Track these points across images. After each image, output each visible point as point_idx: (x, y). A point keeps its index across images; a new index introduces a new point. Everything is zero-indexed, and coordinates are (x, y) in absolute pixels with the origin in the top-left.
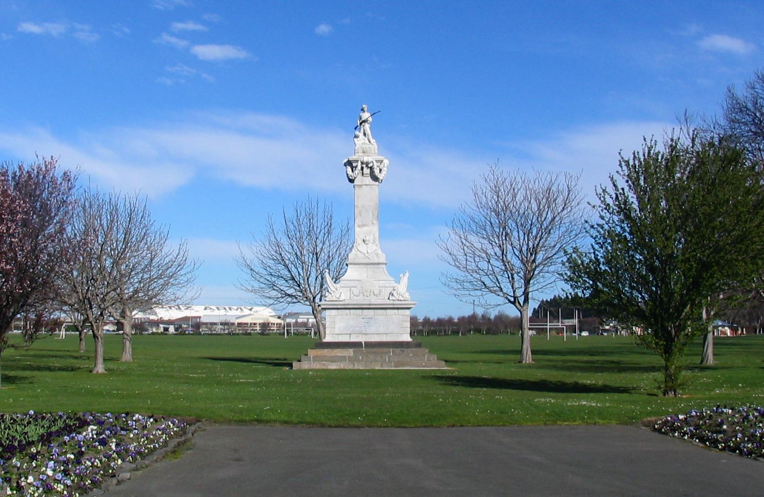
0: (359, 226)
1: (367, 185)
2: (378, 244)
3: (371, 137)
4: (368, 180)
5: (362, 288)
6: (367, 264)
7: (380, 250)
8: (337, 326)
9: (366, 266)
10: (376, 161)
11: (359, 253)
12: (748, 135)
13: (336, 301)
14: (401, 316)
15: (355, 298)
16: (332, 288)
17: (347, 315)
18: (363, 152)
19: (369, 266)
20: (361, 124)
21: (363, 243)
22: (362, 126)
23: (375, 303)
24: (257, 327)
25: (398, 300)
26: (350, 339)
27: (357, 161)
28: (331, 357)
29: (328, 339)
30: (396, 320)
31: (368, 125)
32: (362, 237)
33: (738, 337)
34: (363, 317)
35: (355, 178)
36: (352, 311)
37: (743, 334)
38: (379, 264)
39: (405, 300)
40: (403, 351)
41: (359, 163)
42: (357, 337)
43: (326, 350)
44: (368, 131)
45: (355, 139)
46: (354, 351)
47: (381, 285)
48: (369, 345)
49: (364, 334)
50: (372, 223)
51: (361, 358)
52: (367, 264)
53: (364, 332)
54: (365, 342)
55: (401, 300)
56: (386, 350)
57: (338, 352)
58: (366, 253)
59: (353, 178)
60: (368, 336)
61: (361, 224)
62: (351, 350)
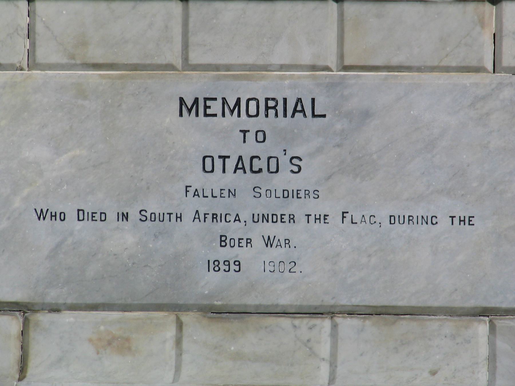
34: (192, 87)
49: (217, 312)
53: (209, 284)
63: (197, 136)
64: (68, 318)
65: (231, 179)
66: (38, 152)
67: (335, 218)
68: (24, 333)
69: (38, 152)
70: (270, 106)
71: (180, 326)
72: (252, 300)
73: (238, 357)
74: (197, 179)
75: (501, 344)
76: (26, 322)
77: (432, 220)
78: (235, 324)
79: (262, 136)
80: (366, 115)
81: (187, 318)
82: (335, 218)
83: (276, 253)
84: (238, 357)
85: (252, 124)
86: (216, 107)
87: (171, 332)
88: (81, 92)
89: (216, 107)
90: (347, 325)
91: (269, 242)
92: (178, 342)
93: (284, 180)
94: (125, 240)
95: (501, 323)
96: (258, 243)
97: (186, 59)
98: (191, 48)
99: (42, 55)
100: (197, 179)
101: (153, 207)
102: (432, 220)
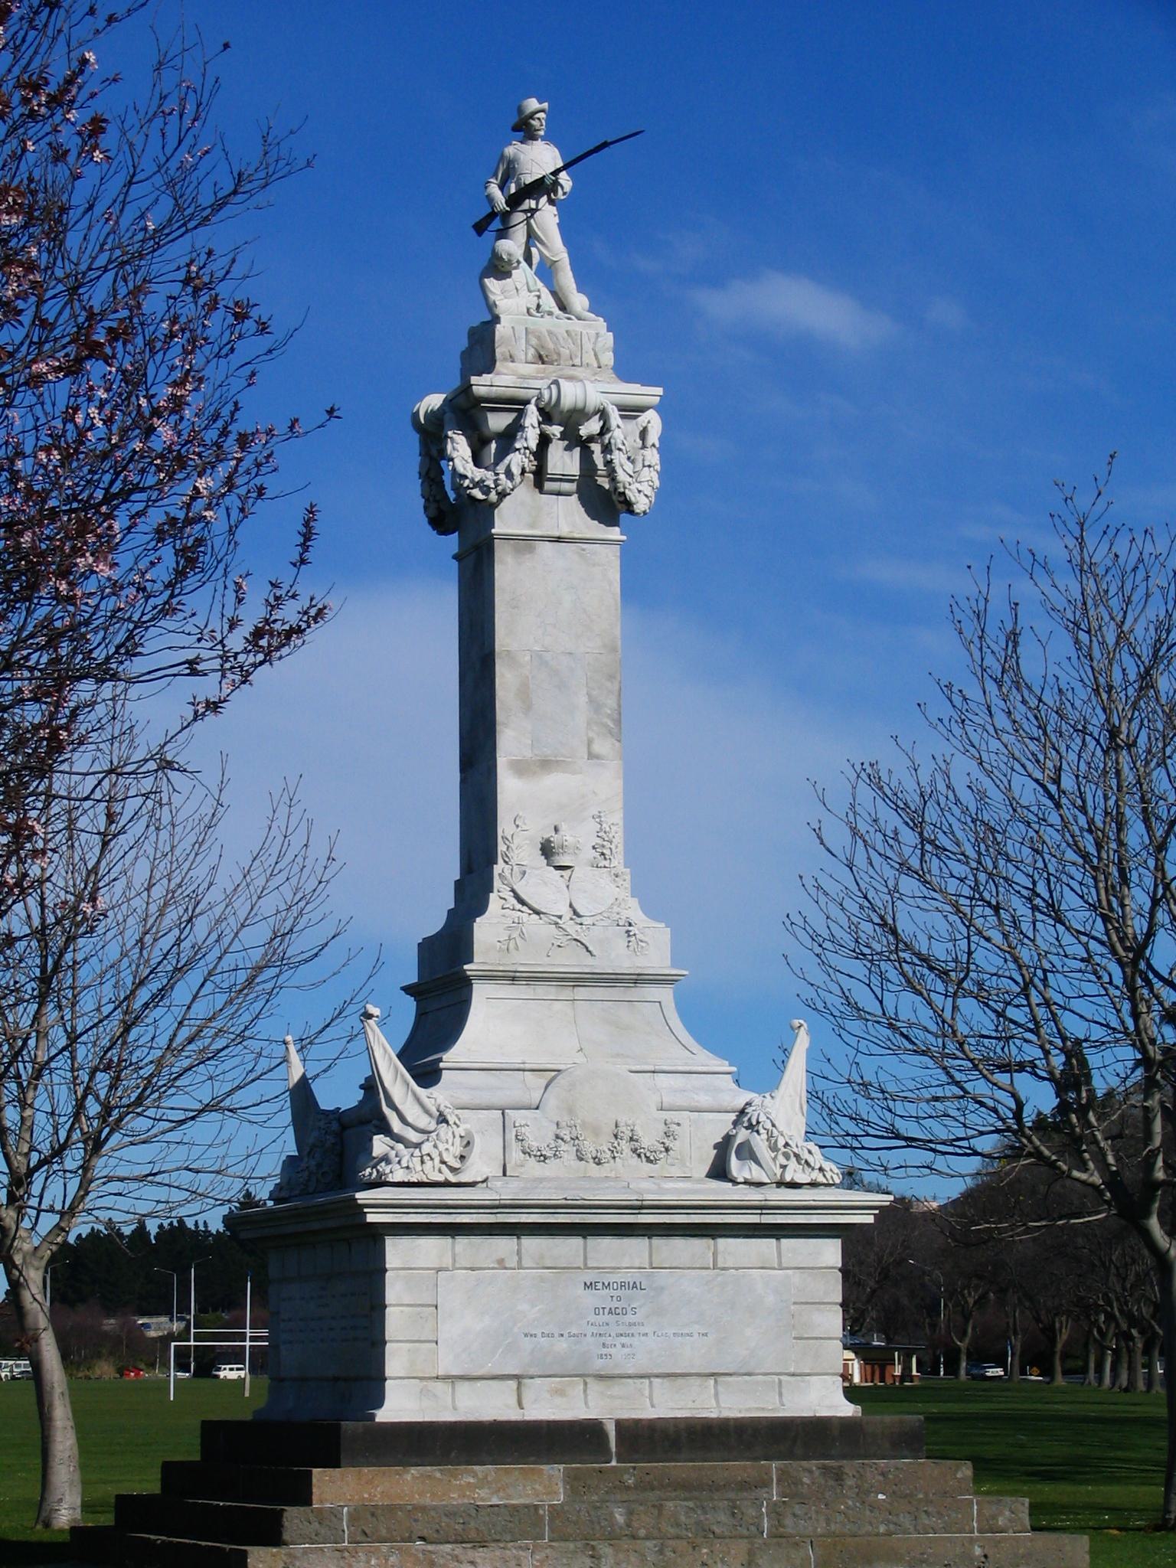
0: (521, 768)
1: (559, 540)
2: (621, 869)
3: (567, 279)
4: (567, 514)
5: (571, 1111)
6: (578, 980)
7: (634, 903)
8: (449, 1331)
9: (567, 993)
10: (621, 408)
11: (526, 917)
12: (107, 490)
13: (447, 1184)
14: (796, 1277)
15: (534, 1169)
16: (412, 1113)
17: (501, 1264)
18: (541, 359)
19: (582, 993)
20: (514, 201)
21: (543, 860)
22: (518, 217)
23: (669, 1198)
24: (242, 1337)
25: (780, 1184)
26: (520, 1405)
27: (516, 405)
28: (451, 1513)
29: (399, 1406)
30: (770, 1299)
31: (554, 209)
32: (536, 829)
33: (893, 1386)
34: (589, 1276)
35: (502, 495)
36: (530, 1243)
37: (911, 1378)
38: (638, 980)
39: (814, 1185)
40: (839, 1477)
41: (532, 417)
42: (560, 1392)
43: (413, 1470)
44: (556, 248)
45: (491, 283)
46: (571, 1479)
47: (667, 1100)
48: (646, 1439)
49: (600, 1377)
50: (591, 756)
51: (620, 1519)
52: (578, 980)
53: (598, 1365)
54: (619, 1424)
55: (794, 1185)
56: (739, 1468)
57: (483, 1482)
58: (567, 913)
59: (493, 497)
60: (617, 1389)
61: (528, 754)
62: (555, 1471)
63: (590, 1299)
64: (538, 1381)
65: (607, 1318)
66: (524, 1307)
67: (651, 1334)
68: (519, 1388)
69: (524, 1307)
70: (622, 1285)
71: (585, 1384)
72: (617, 1372)
73: (611, 1397)
74: (592, 1318)
75: (720, 1389)
76: (519, 1384)
77: (690, 1335)
78: (609, 1382)
79: (619, 1298)
80: (662, 1288)
81: (588, 1380)
82: (651, 1334)
83: (626, 1350)
84: (611, 1397)
85: (615, 1293)
86: (600, 1286)
87: (582, 1387)
88: (542, 1279)
89: (600, 1286)
90: (656, 1381)
91: (623, 1346)
92: (585, 1391)
93: (630, 1318)
94: (562, 1345)
95: (721, 1379)
96: (619, 1346)
97: (585, 1264)
98: (446, 1241)
99: (525, 1263)
100: (592, 1318)
101: (574, 1331)
102: (690, 1335)
